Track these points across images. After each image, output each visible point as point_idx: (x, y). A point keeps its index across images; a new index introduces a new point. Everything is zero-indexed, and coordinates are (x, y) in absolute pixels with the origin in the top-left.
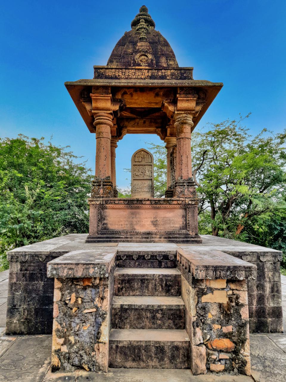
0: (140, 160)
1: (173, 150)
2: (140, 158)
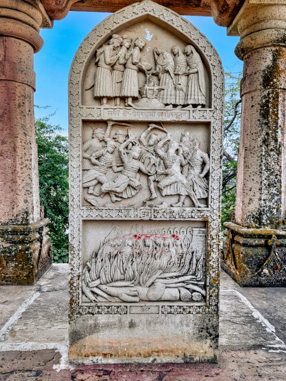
0: (131, 88)
1: (274, 60)
2: (132, 75)
